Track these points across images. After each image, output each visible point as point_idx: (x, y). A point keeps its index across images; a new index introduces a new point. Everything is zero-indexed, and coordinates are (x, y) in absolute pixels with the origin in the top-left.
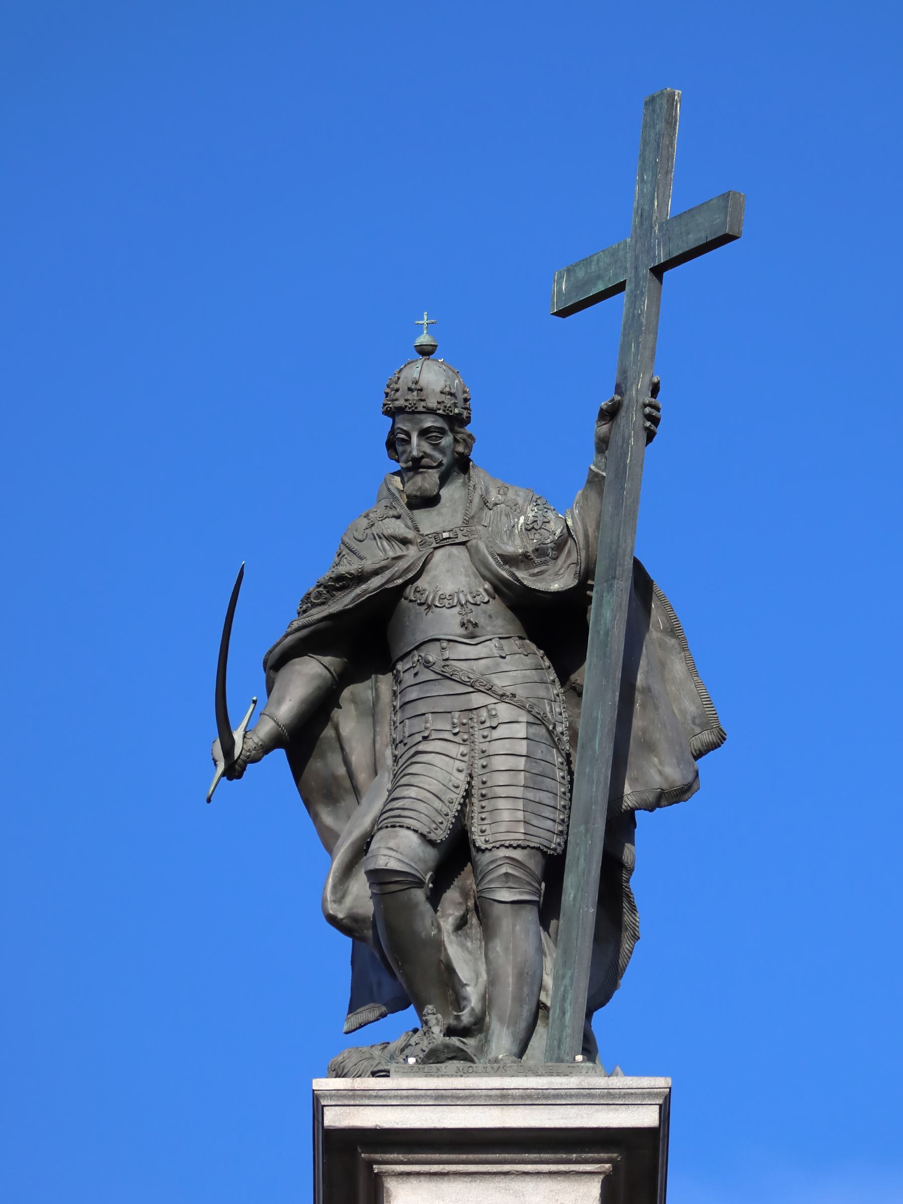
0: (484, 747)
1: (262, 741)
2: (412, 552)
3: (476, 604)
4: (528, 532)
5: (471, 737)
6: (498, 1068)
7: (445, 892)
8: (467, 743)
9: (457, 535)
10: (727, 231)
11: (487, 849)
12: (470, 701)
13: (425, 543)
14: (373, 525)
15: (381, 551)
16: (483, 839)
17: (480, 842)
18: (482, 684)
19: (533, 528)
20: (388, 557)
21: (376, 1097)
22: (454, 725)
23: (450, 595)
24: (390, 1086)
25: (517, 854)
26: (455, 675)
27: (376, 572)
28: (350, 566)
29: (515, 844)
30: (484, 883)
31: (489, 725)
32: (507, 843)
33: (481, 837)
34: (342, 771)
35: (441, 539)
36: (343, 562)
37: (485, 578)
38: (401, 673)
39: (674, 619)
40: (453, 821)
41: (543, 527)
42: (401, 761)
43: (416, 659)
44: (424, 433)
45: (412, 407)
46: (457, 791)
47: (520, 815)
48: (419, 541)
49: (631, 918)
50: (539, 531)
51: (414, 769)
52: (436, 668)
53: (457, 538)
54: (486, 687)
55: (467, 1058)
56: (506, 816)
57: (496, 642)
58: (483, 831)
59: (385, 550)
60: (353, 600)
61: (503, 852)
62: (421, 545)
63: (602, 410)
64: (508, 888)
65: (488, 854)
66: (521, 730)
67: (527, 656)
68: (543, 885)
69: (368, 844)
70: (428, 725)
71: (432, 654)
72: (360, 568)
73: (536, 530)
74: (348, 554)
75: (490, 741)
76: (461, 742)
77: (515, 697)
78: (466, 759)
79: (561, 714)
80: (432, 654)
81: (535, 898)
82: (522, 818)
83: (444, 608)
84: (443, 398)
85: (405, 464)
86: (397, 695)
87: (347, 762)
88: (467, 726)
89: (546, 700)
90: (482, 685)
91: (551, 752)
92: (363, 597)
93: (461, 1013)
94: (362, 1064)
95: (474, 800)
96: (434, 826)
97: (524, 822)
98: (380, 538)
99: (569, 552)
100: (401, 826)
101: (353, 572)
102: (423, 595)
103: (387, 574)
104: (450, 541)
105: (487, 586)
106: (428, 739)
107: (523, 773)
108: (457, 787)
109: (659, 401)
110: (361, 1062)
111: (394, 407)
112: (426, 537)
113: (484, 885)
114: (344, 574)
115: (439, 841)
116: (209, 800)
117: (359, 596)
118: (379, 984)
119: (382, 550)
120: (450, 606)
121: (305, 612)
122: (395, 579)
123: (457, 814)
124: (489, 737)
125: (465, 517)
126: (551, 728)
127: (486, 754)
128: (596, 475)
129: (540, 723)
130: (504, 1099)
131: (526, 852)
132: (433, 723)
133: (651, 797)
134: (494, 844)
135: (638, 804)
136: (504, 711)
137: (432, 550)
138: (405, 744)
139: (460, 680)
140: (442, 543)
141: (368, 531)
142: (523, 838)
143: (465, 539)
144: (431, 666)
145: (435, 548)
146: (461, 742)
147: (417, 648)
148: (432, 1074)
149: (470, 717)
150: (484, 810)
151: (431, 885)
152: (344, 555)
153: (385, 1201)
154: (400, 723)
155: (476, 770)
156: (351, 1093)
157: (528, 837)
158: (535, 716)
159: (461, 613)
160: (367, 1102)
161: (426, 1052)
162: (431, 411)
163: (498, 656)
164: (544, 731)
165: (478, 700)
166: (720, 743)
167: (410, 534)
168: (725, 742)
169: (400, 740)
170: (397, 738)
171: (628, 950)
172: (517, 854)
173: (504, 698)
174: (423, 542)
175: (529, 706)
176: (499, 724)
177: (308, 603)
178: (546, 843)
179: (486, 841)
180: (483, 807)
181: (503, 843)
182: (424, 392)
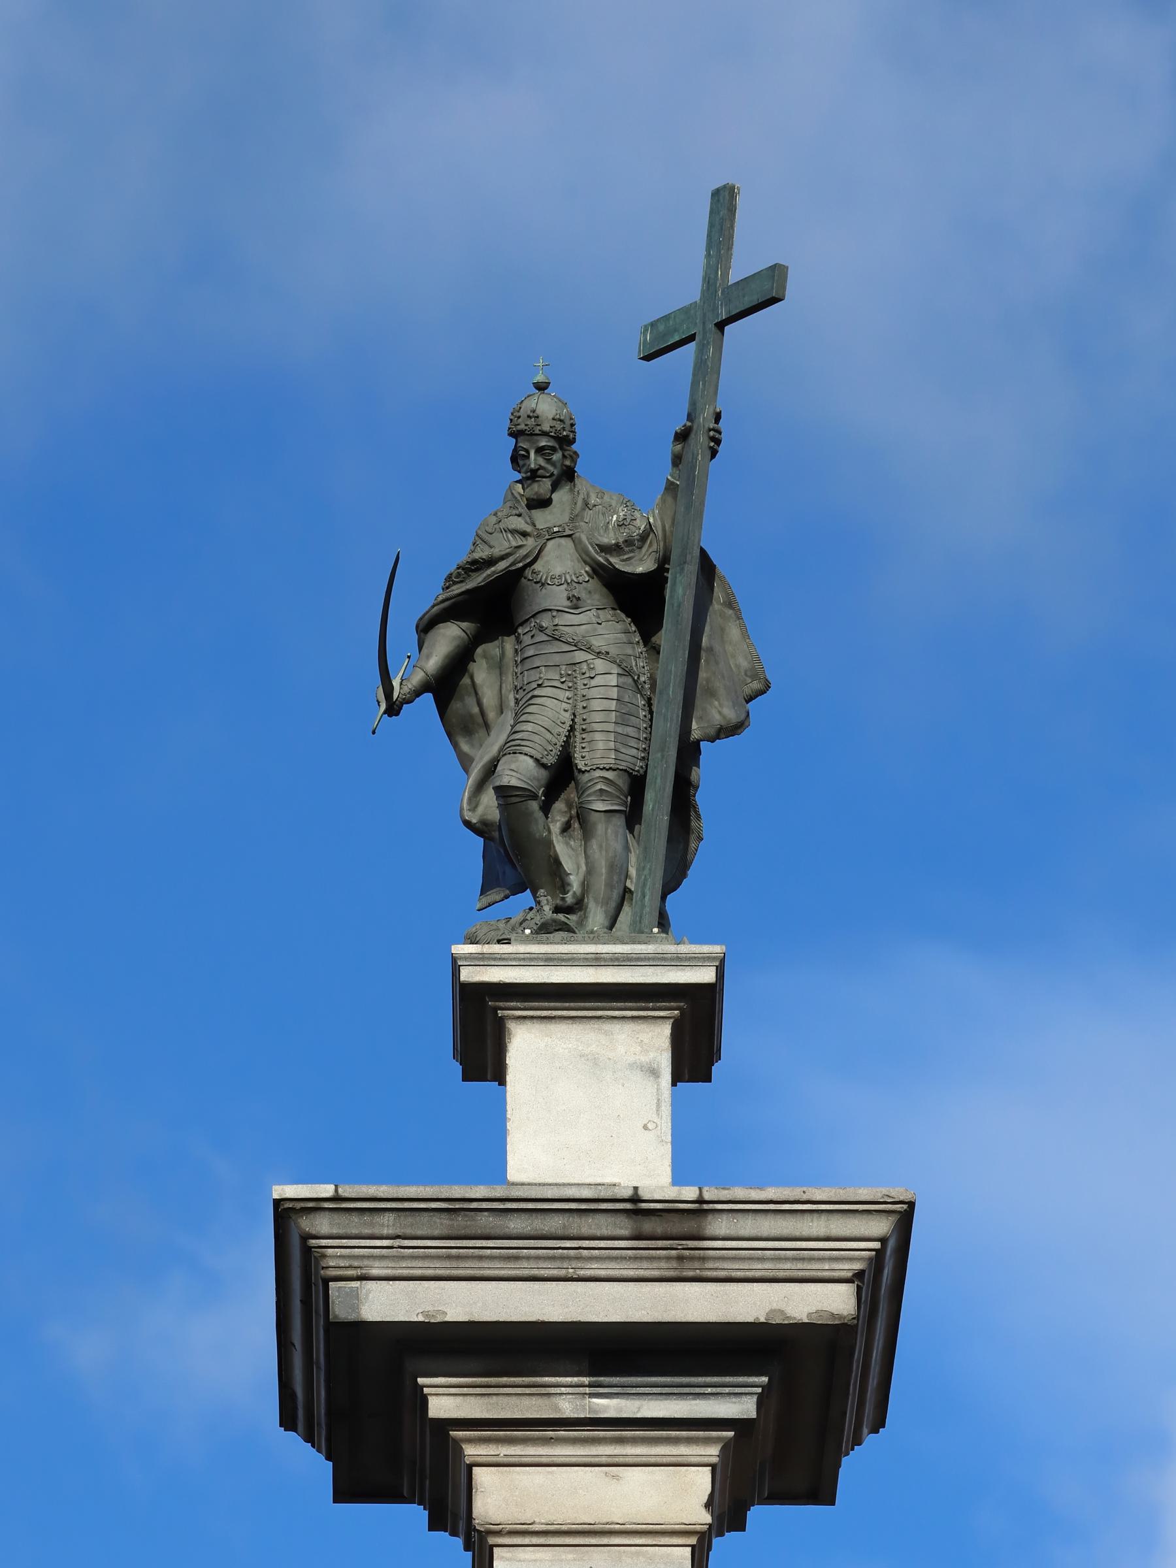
2: (530, 542)
3: (579, 583)
6: (594, 938)
11: (586, 770)
16: (583, 762)
17: (581, 766)
19: (623, 524)
22: (561, 676)
25: (609, 775)
27: (502, 558)
28: (482, 553)
29: (607, 767)
32: (601, 766)
34: (476, 710)
37: (586, 562)
43: (532, 625)
44: (540, 451)
52: (547, 631)
56: (601, 745)
57: (594, 612)
58: (583, 757)
60: (483, 581)
61: (598, 773)
63: (676, 433)
65: (587, 775)
66: (613, 680)
67: (618, 622)
68: (629, 798)
69: (496, 766)
70: (542, 675)
74: (481, 544)
76: (567, 688)
78: (570, 701)
79: (644, 667)
83: (555, 586)
87: (479, 704)
96: (546, 753)
98: (506, 531)
99: (651, 543)
101: (484, 557)
103: (511, 559)
104: (560, 534)
105: (588, 569)
108: (563, 723)
113: (584, 798)
116: (374, 732)
117: (489, 576)
118: (504, 873)
121: (447, 588)
123: (563, 744)
126: (636, 678)
127: (586, 698)
128: (672, 483)
130: (597, 961)
131: (615, 773)
136: (600, 665)
137: (545, 541)
138: (524, 690)
140: (553, 536)
143: (571, 532)
145: (548, 540)
151: (543, 798)
156: (481, 956)
160: (493, 963)
162: (545, 434)
164: (630, 680)
165: (580, 656)
167: (529, 529)
172: (609, 775)
177: (450, 581)
181: (598, 766)
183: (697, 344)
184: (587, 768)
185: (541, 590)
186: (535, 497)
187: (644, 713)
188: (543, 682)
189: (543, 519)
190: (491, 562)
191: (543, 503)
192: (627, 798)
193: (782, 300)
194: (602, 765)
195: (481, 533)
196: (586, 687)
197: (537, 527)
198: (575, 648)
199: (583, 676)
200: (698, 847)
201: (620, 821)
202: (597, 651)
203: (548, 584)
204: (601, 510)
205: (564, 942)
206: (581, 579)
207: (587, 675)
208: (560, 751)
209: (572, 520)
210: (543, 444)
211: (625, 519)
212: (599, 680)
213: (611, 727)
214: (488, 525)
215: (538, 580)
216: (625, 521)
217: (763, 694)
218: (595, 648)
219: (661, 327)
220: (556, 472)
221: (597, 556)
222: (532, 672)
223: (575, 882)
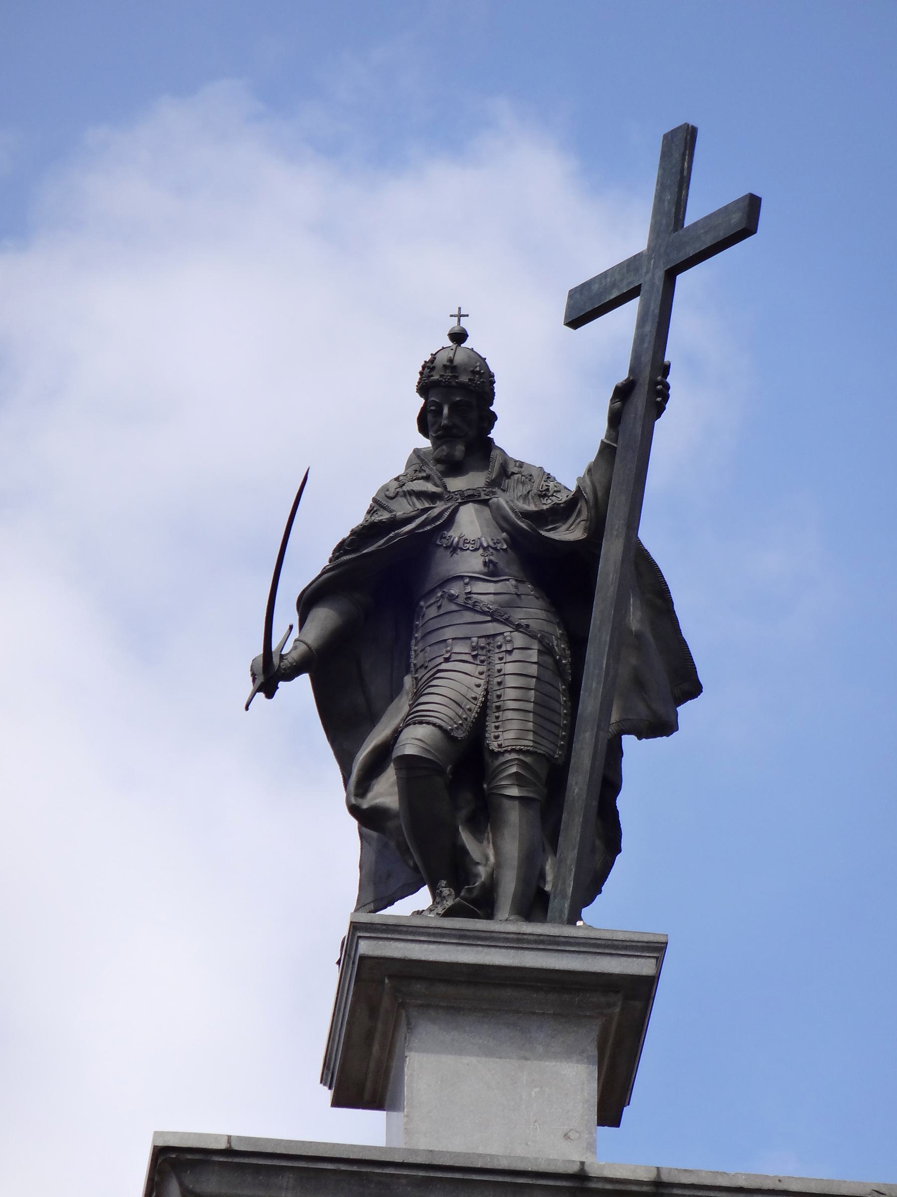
2: (440, 507)
8: (485, 663)
11: (499, 752)
14: (404, 485)
16: (496, 744)
19: (545, 494)
22: (474, 648)
23: (473, 541)
25: (528, 759)
31: (505, 649)
37: (503, 530)
38: (424, 609)
40: (471, 726)
41: (554, 494)
42: (420, 683)
46: (475, 702)
47: (530, 726)
48: (446, 497)
50: (550, 498)
51: (434, 682)
52: (461, 601)
57: (514, 582)
59: (414, 504)
66: (534, 656)
69: (397, 737)
71: (455, 589)
73: (549, 497)
75: (505, 663)
76: (479, 663)
78: (483, 676)
80: (455, 589)
83: (469, 551)
90: (500, 615)
93: (475, 885)
103: (418, 521)
106: (451, 660)
111: (430, 382)
112: (453, 494)
116: (247, 708)
119: (411, 504)
136: (519, 639)
138: (426, 667)
142: (532, 745)
150: (499, 720)
151: (451, 776)
154: (421, 651)
156: (384, 927)
157: (536, 745)
165: (493, 628)
172: (528, 759)
174: (450, 497)
178: (551, 753)
183: (641, 300)
188: (450, 655)
189: (456, 484)
190: (395, 523)
194: (519, 747)
196: (502, 661)
198: (489, 618)
206: (499, 546)
207: (503, 649)
212: (516, 655)
213: (530, 706)
214: (388, 490)
218: (513, 620)
221: (517, 520)
222: (436, 647)
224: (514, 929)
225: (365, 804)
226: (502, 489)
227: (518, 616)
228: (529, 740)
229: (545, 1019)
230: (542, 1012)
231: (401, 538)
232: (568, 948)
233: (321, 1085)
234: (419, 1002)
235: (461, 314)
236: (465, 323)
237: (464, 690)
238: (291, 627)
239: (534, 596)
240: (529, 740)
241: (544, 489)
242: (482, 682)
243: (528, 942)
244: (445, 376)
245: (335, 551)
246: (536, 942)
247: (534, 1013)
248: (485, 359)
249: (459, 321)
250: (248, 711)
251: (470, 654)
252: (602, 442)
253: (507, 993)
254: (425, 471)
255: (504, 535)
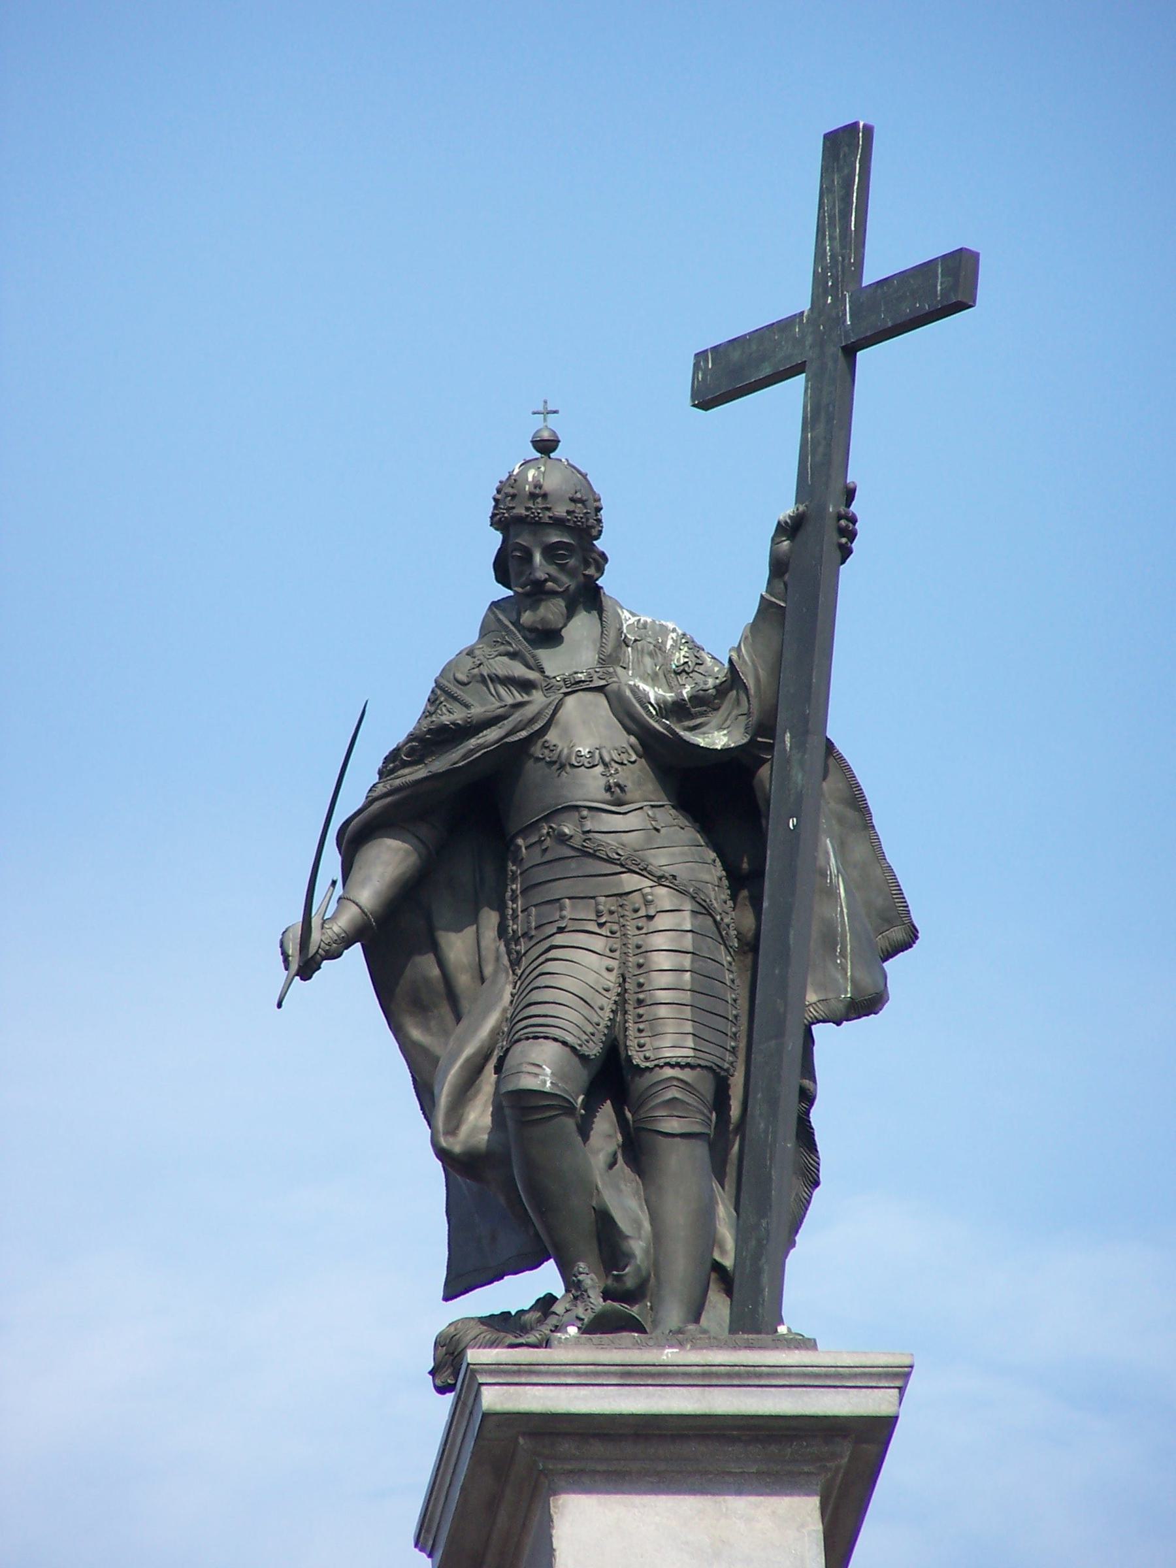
0: (637, 940)
1: (345, 932)
2: (538, 698)
3: (622, 764)
4: (678, 677)
5: (622, 928)
6: (678, 1338)
7: (593, 1122)
9: (592, 677)
10: (959, 300)
11: (647, 1068)
12: (621, 882)
13: (552, 687)
15: (494, 696)
16: (641, 1055)
17: (637, 1060)
18: (634, 862)
19: (684, 671)
20: (506, 703)
21: (546, 1373)
22: (599, 914)
24: (564, 1360)
26: (601, 852)
29: (683, 1061)
30: (647, 1109)
31: (644, 914)
32: (673, 1061)
33: (639, 1053)
34: (436, 972)
35: (573, 682)
36: (441, 710)
39: (855, 787)
41: (696, 669)
43: (545, 831)
44: (550, 552)
45: (536, 517)
47: (688, 1027)
48: (544, 685)
49: (812, 1162)
51: (550, 967)
52: (573, 842)
53: (591, 681)
54: (639, 866)
55: (641, 1329)
58: (641, 1046)
60: (464, 757)
61: (669, 1072)
62: (546, 690)
64: (677, 1116)
67: (683, 828)
68: (714, 1114)
70: (564, 913)
72: (469, 718)
73: (688, 673)
74: (446, 700)
75: (646, 934)
76: (609, 934)
77: (676, 880)
78: (616, 955)
79: (725, 902)
81: (706, 1131)
82: (690, 1030)
83: (583, 768)
84: (571, 507)
85: (523, 588)
86: (517, 877)
87: (441, 963)
88: (616, 914)
89: (709, 884)
90: (633, 864)
91: (718, 949)
92: (478, 752)
93: (624, 1272)
94: (484, 1337)
95: (629, 1007)
96: (586, 1037)
97: (694, 1035)
98: (492, 680)
100: (546, 1038)
101: (459, 722)
102: (554, 752)
103: (508, 725)
104: (584, 686)
106: (566, 930)
107: (689, 973)
108: (607, 990)
109: (854, 508)
110: (483, 1335)
112: (554, 680)
113: (642, 1114)
114: (448, 725)
115: (593, 1057)
116: (279, 1005)
120: (591, 765)
121: (392, 771)
122: (518, 732)
123: (609, 1024)
124: (645, 928)
125: (601, 656)
126: (718, 918)
127: (642, 950)
129: (706, 912)
130: (708, 1377)
132: (569, 910)
133: (840, 1008)
134: (656, 1062)
135: (827, 1015)
136: (664, 896)
137: (562, 695)
139: (605, 857)
140: (575, 686)
141: (476, 671)
143: (603, 683)
144: (567, 840)
145: (566, 694)
146: (609, 934)
147: (547, 818)
148: (604, 1347)
149: (621, 904)
152: (442, 702)
153: (551, 1505)
155: (630, 970)
156: (515, 1368)
158: (698, 903)
159: (604, 773)
160: (535, 1380)
161: (586, 1320)
162: (558, 523)
163: (651, 827)
164: (709, 921)
165: (631, 881)
166: (912, 942)
167: (533, 675)
168: (917, 942)
169: (523, 932)
170: (519, 930)
171: (805, 1199)
173: (663, 880)
174: (549, 686)
175: (694, 890)
176: (658, 912)
177: (394, 761)
179: (647, 1059)
180: (640, 1016)
181: (668, 1060)
182: (549, 498)
184: (648, 1064)
185: (559, 776)
186: (540, 627)
187: (731, 976)
189: (555, 663)
191: (550, 637)
192: (711, 1113)
193: (971, 306)
194: (674, 1059)
195: (446, 683)
197: (547, 674)
199: (636, 916)
200: (811, 1197)
201: (700, 1150)
202: (660, 874)
203: (573, 766)
204: (645, 648)
205: (638, 1345)
207: (642, 912)
208: (605, 1035)
209: (603, 661)
210: (555, 539)
211: (687, 663)
212: (662, 921)
215: (554, 759)
216: (686, 666)
217: (907, 949)
219: (736, 355)
220: (572, 587)
223: (638, 1247)
224: (698, 1360)
225: (456, 1145)
226: (622, 667)
227: (660, 860)
228: (689, 1048)
229: (745, 1480)
230: (741, 1470)
231: (486, 750)
232: (774, 1382)
233: (417, 1550)
234: (569, 1467)
235: (549, 409)
236: (556, 425)
237: (591, 978)
238: (334, 883)
239: (679, 826)
240: (689, 1048)
241: (682, 662)
242: (614, 964)
243: (717, 1375)
244: (532, 508)
245: (387, 760)
246: (729, 1375)
247: (729, 1473)
248: (587, 475)
249: (545, 420)
250: (281, 1009)
251: (596, 921)
252: (762, 596)
253: (692, 1448)
254: (510, 644)
255: (633, 739)
